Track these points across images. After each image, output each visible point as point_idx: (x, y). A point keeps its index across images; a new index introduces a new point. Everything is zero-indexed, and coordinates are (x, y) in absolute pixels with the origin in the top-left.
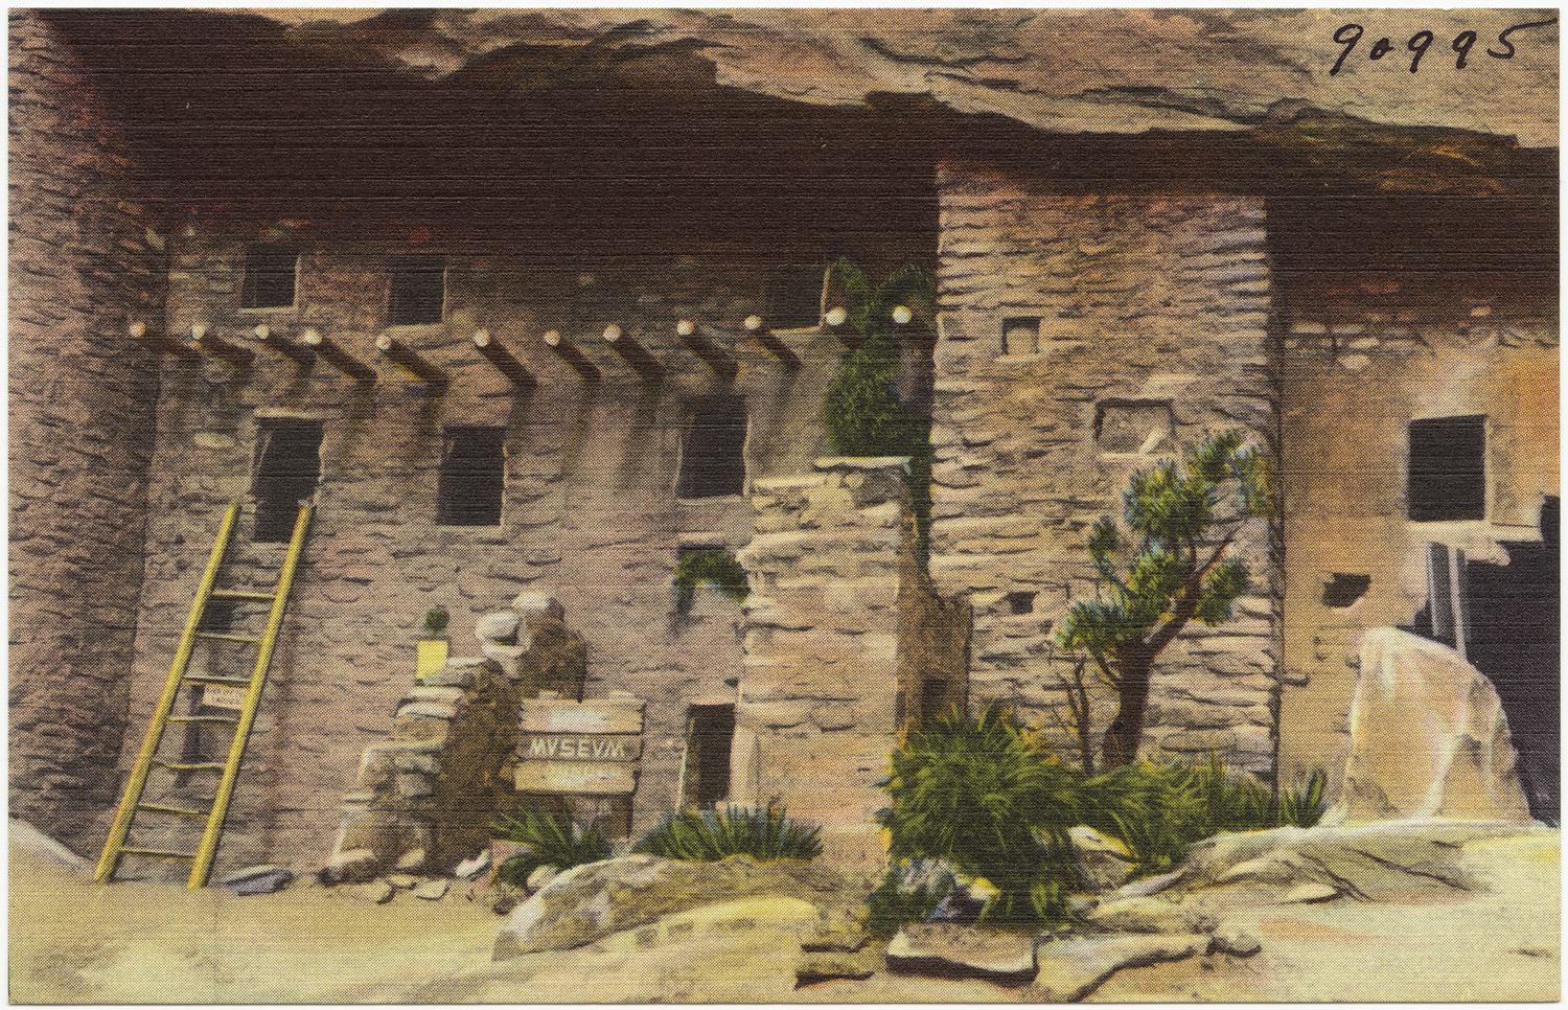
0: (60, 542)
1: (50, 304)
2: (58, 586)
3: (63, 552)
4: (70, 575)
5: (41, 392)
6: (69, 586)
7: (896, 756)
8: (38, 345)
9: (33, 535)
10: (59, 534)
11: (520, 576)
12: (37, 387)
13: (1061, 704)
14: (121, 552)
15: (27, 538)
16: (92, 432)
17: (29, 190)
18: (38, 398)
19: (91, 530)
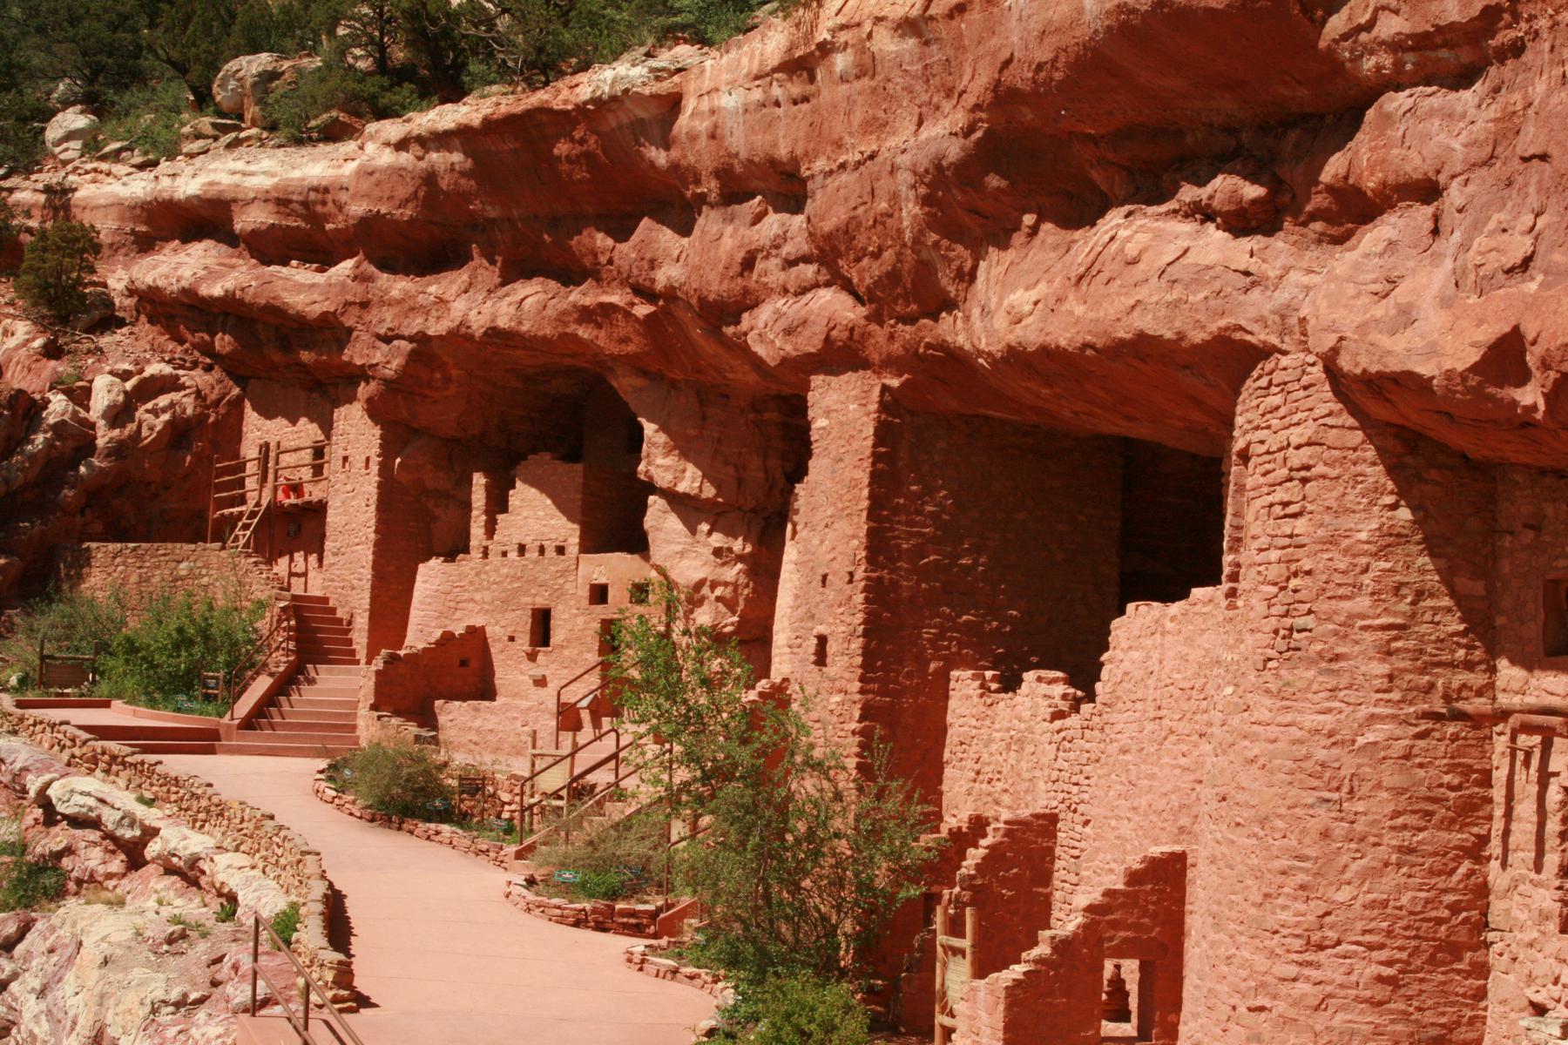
0: (1371, 947)
1: (1347, 692)
2: (1368, 993)
3: (1376, 955)
4: (1380, 979)
5: (1338, 789)
6: (1382, 992)
7: (1218, 228)
8: (1333, 740)
9: (1339, 943)
10: (1368, 938)
11: (1512, 839)
12: (1334, 784)
13: (267, 953)
14: (1454, 950)
15: (1333, 947)
16: (1400, 821)
17: (647, 471)
18: (1336, 796)
19: (1406, 928)
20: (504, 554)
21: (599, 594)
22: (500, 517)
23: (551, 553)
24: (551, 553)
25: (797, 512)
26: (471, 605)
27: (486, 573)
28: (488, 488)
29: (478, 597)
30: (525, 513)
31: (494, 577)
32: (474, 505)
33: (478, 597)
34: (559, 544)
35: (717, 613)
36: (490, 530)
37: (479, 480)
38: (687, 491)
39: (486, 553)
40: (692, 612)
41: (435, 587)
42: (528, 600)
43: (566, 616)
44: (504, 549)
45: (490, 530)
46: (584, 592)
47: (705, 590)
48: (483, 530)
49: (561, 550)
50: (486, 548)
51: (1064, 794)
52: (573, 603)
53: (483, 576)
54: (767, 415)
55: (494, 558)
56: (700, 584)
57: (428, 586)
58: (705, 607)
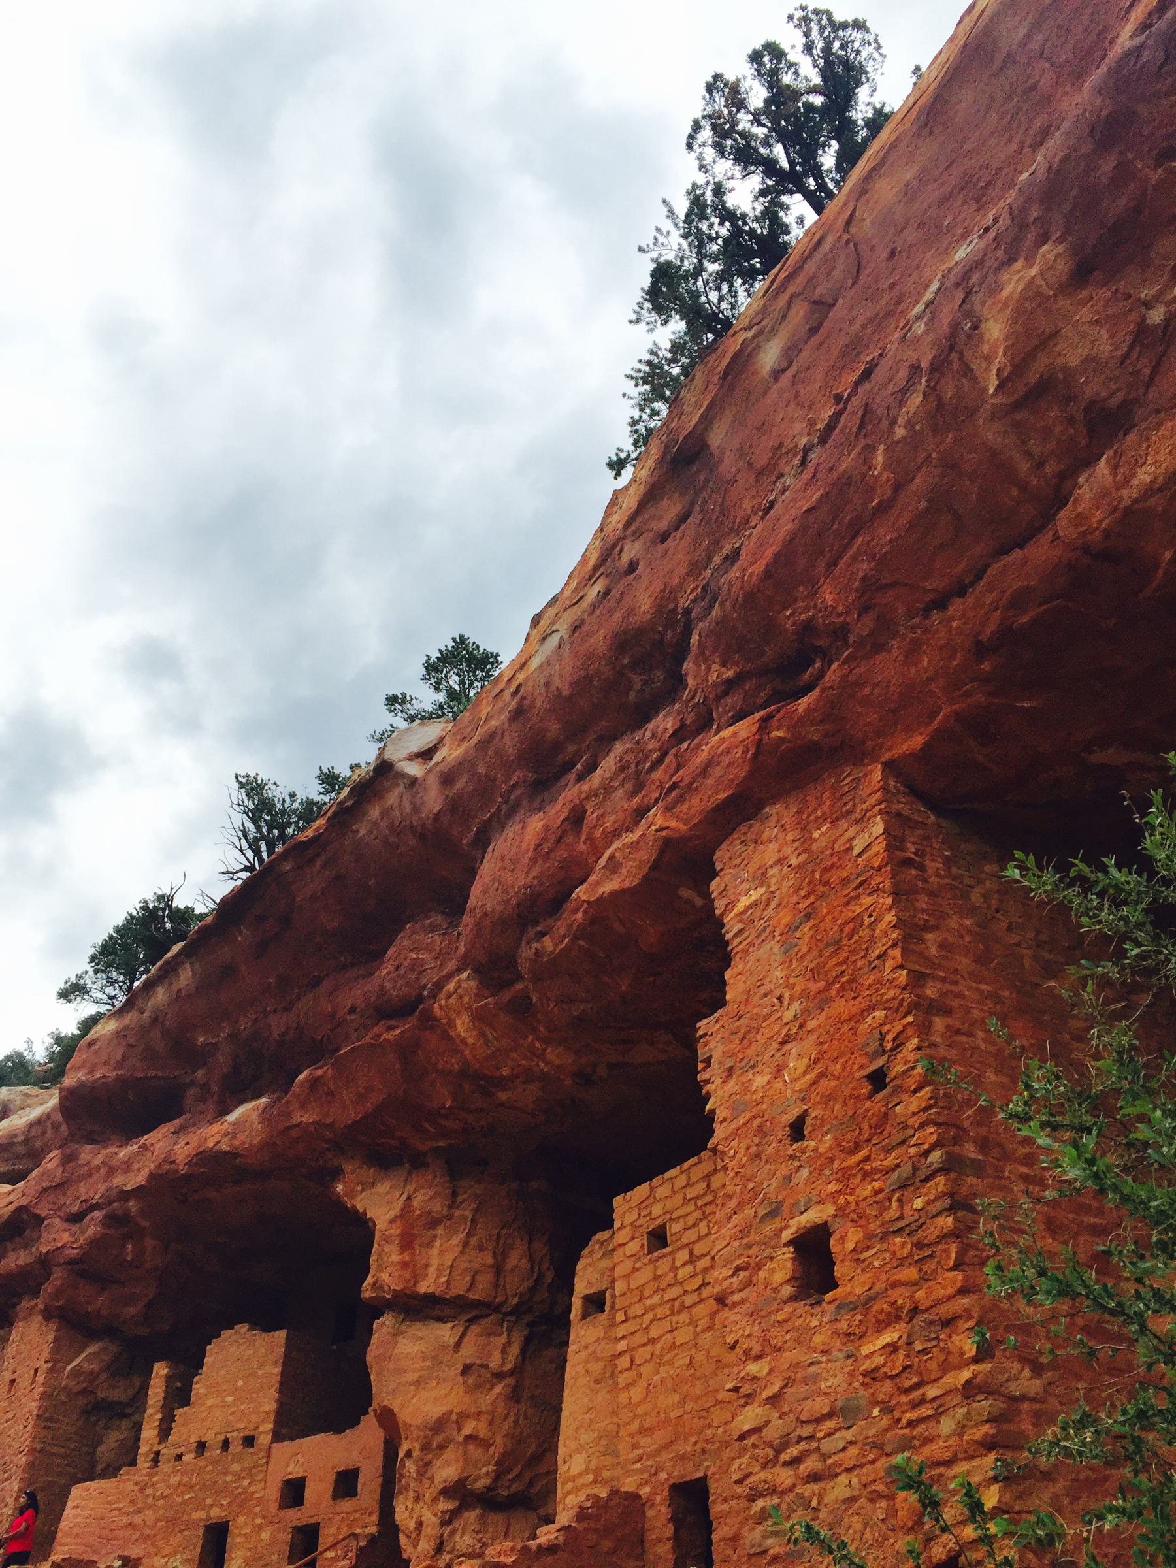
20: (179, 1457)
21: (294, 1492)
22: (179, 1412)
23: (236, 1447)
24: (236, 1447)
25: (549, 1541)
26: (128, 1533)
27: (154, 1484)
28: (169, 1379)
29: (137, 1519)
30: (210, 1402)
31: (161, 1489)
32: (150, 1402)
33: (137, 1519)
34: (247, 1433)
35: (467, 1461)
36: (165, 1432)
37: (160, 1370)
38: (430, 1290)
39: (156, 1459)
40: (428, 1464)
41: (86, 1513)
42: (201, 1514)
43: (247, 1530)
44: (179, 1451)
45: (165, 1432)
46: (273, 1492)
47: (451, 1431)
48: (156, 1432)
49: (249, 1441)
50: (158, 1453)
51: (1099, 1559)
52: (257, 1509)
53: (149, 1491)
54: (534, 1185)
55: (165, 1467)
56: (438, 1426)
57: (79, 1511)
58: (450, 1453)
